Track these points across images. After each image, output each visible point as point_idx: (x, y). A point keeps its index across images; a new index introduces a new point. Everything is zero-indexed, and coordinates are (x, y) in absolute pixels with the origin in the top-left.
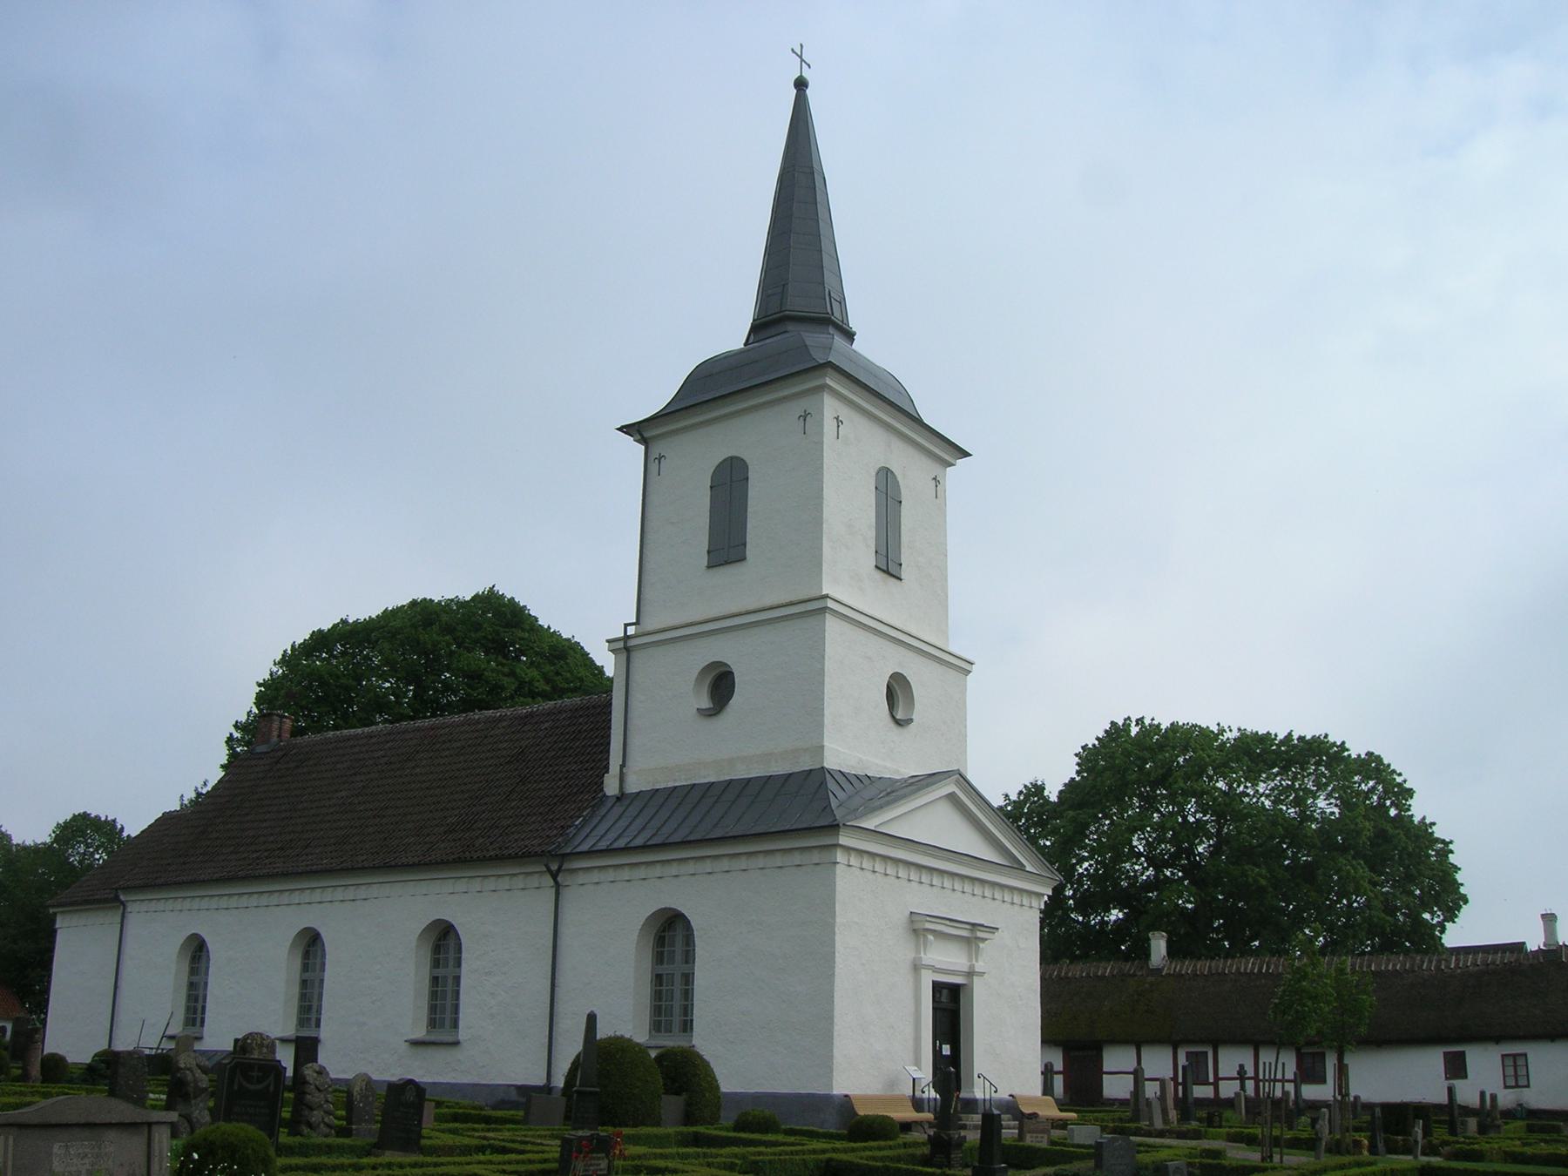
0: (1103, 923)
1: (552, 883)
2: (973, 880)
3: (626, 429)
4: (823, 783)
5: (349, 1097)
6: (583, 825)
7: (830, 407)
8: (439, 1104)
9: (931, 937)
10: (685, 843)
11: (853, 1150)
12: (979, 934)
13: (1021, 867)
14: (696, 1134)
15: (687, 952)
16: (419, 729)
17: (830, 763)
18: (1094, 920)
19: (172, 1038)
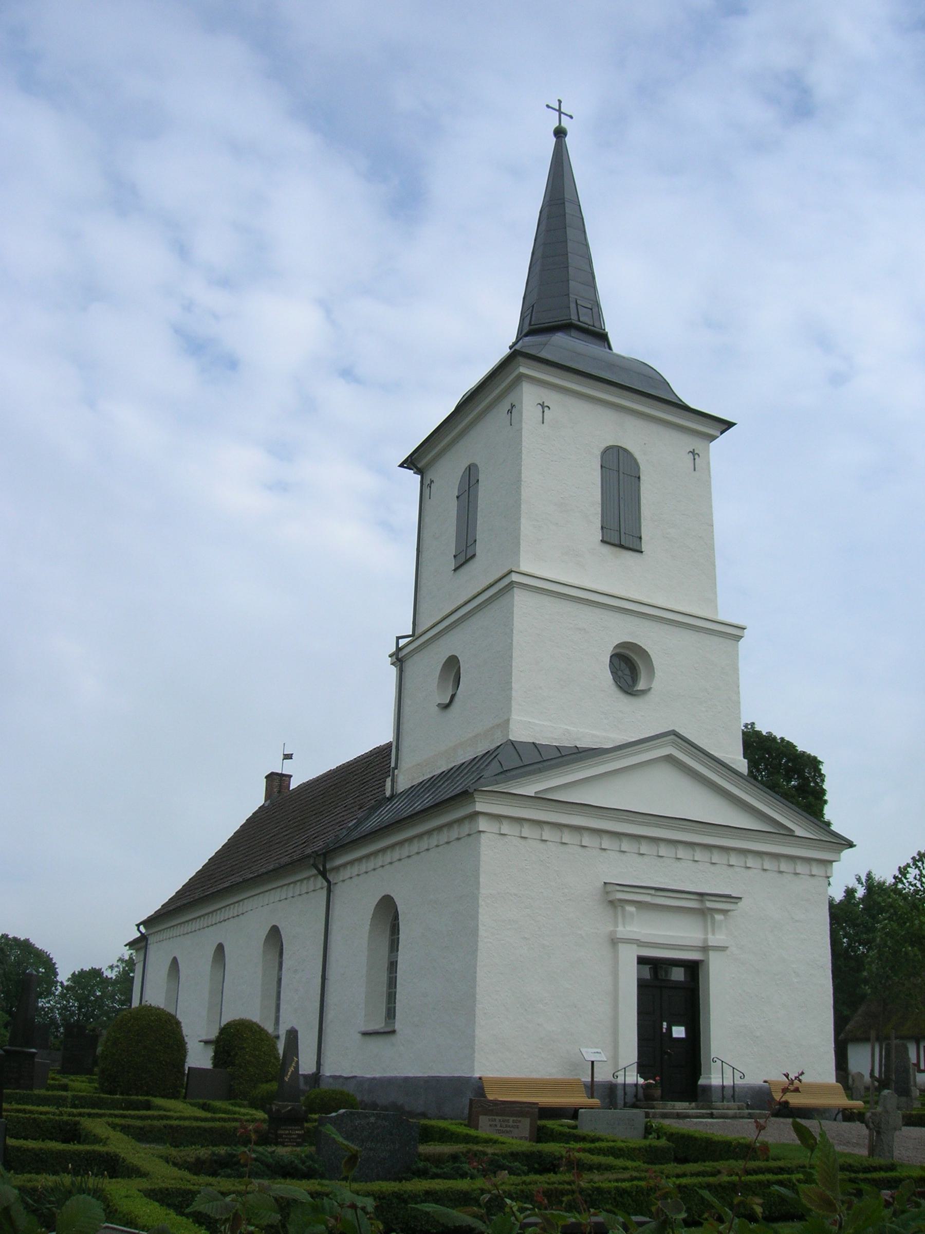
3: (401, 466)
12: (709, 905)
13: (790, 833)
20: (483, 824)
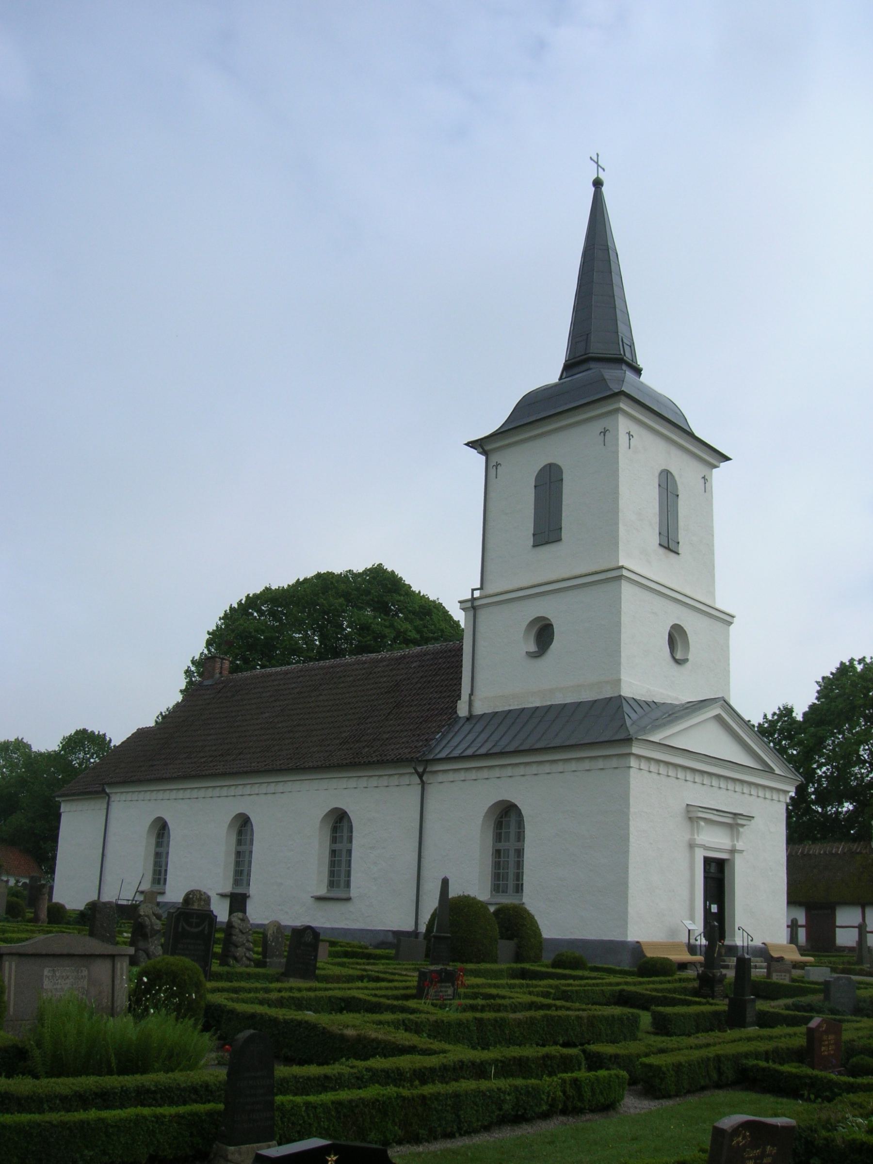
0: (838, 813)
1: (419, 781)
2: (735, 780)
3: (472, 444)
4: (620, 707)
5: (264, 937)
6: (441, 739)
7: (623, 425)
8: (333, 944)
9: (702, 823)
10: (517, 752)
11: (641, 983)
12: (740, 822)
13: (772, 771)
14: (523, 969)
15: (519, 832)
16: (322, 668)
17: (626, 692)
18: (831, 810)
19: (142, 892)
20: (633, 762)
